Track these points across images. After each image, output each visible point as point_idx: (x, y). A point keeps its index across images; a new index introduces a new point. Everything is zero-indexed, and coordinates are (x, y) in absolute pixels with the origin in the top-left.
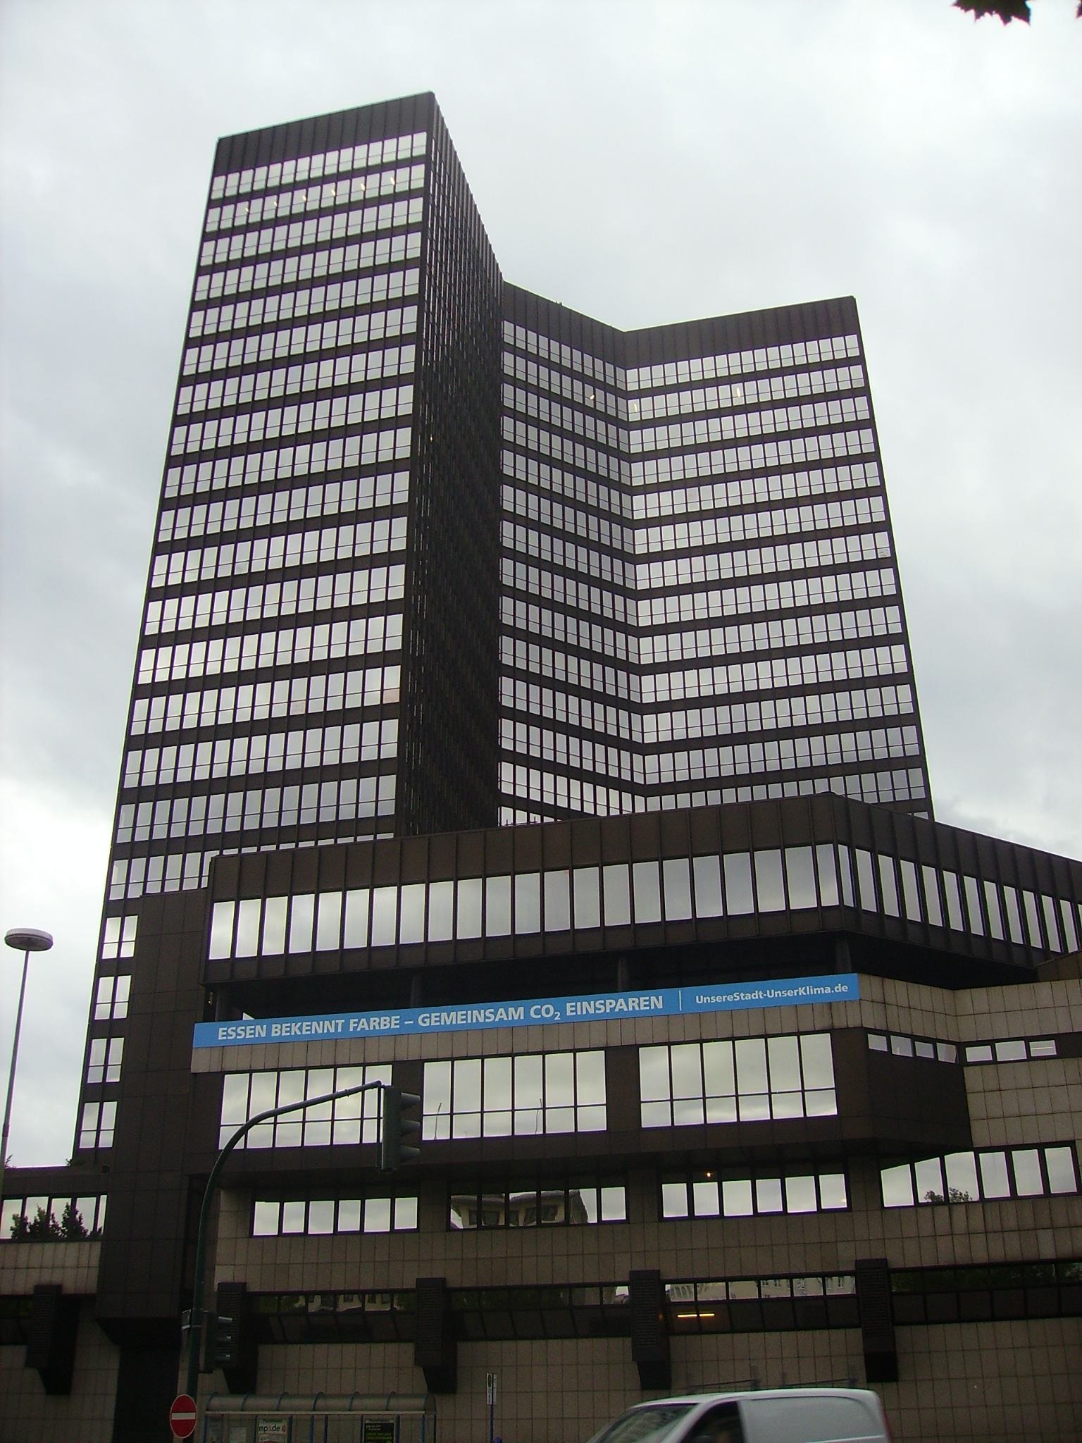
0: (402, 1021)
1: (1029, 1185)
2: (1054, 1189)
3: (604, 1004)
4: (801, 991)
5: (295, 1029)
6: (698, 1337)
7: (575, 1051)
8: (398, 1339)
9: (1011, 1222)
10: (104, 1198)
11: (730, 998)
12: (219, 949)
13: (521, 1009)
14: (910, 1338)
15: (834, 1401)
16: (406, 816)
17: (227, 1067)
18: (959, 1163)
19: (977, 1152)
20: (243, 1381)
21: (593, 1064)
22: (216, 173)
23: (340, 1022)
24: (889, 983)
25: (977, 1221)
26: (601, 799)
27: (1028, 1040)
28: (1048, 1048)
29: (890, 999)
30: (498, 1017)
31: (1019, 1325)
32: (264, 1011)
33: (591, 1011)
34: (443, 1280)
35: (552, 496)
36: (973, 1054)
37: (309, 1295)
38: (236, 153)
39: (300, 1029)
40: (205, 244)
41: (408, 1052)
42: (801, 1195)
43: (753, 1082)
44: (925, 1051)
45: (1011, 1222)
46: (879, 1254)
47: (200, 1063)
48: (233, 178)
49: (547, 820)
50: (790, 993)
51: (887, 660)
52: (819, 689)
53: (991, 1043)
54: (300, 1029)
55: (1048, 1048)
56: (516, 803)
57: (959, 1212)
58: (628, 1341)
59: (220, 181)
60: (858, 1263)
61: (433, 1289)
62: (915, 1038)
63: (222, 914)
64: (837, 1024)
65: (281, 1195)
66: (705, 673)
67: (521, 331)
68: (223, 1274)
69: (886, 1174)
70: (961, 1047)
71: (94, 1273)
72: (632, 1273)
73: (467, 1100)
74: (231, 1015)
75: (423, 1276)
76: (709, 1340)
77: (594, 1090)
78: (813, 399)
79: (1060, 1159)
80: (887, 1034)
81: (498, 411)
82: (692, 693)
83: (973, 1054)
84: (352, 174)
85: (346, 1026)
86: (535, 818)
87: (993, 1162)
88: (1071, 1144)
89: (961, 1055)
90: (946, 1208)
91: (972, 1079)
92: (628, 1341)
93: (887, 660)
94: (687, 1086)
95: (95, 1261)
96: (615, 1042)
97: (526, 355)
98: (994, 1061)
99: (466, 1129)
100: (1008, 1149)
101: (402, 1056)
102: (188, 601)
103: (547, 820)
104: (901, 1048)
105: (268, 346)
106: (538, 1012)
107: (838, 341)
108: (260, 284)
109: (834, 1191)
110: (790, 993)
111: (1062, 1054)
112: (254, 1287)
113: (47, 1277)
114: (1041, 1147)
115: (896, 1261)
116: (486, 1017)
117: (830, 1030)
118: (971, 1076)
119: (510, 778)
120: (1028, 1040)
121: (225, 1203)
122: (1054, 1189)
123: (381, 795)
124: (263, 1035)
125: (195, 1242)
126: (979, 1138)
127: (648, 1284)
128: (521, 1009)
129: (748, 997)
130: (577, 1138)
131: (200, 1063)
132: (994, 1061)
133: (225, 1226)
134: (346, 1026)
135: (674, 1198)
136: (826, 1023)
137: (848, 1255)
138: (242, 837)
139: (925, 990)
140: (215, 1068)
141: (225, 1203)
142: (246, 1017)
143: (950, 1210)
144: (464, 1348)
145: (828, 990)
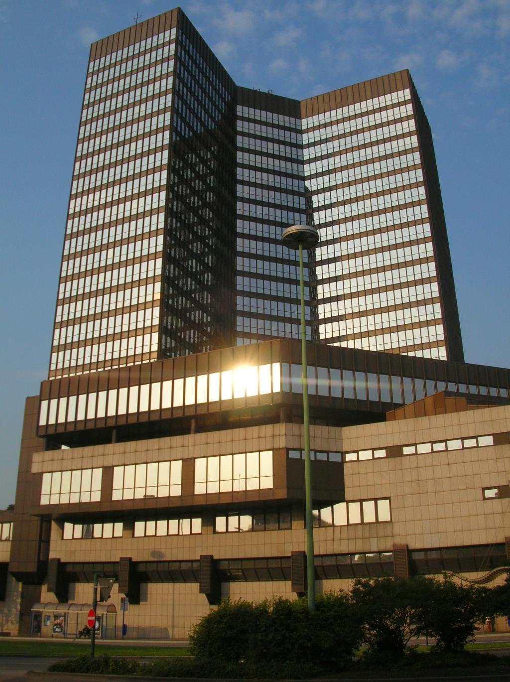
1: (369, 518)
2: (365, 521)
9: (352, 535)
10: (12, 524)
16: (162, 352)
17: (44, 471)
18: (340, 508)
19: (348, 502)
25: (345, 535)
27: (432, 443)
28: (382, 453)
35: (280, 174)
37: (353, 554)
45: (359, 535)
47: (35, 469)
55: (407, 451)
57: (337, 530)
58: (199, 584)
70: (343, 454)
71: (9, 553)
73: (213, 476)
75: (123, 556)
77: (98, 485)
78: (278, 127)
79: (384, 505)
83: (350, 457)
87: (355, 507)
88: (388, 498)
89: (343, 458)
90: (332, 528)
91: (347, 469)
92: (199, 584)
94: (213, 476)
95: (9, 549)
96: (185, 457)
100: (361, 501)
101: (106, 464)
105: (118, 118)
112: (63, 560)
114: (361, 501)
121: (54, 525)
122: (365, 521)
123: (151, 343)
125: (44, 541)
131: (35, 469)
136: (271, 447)
140: (40, 471)
141: (54, 525)
143: (333, 529)
144: (224, 585)
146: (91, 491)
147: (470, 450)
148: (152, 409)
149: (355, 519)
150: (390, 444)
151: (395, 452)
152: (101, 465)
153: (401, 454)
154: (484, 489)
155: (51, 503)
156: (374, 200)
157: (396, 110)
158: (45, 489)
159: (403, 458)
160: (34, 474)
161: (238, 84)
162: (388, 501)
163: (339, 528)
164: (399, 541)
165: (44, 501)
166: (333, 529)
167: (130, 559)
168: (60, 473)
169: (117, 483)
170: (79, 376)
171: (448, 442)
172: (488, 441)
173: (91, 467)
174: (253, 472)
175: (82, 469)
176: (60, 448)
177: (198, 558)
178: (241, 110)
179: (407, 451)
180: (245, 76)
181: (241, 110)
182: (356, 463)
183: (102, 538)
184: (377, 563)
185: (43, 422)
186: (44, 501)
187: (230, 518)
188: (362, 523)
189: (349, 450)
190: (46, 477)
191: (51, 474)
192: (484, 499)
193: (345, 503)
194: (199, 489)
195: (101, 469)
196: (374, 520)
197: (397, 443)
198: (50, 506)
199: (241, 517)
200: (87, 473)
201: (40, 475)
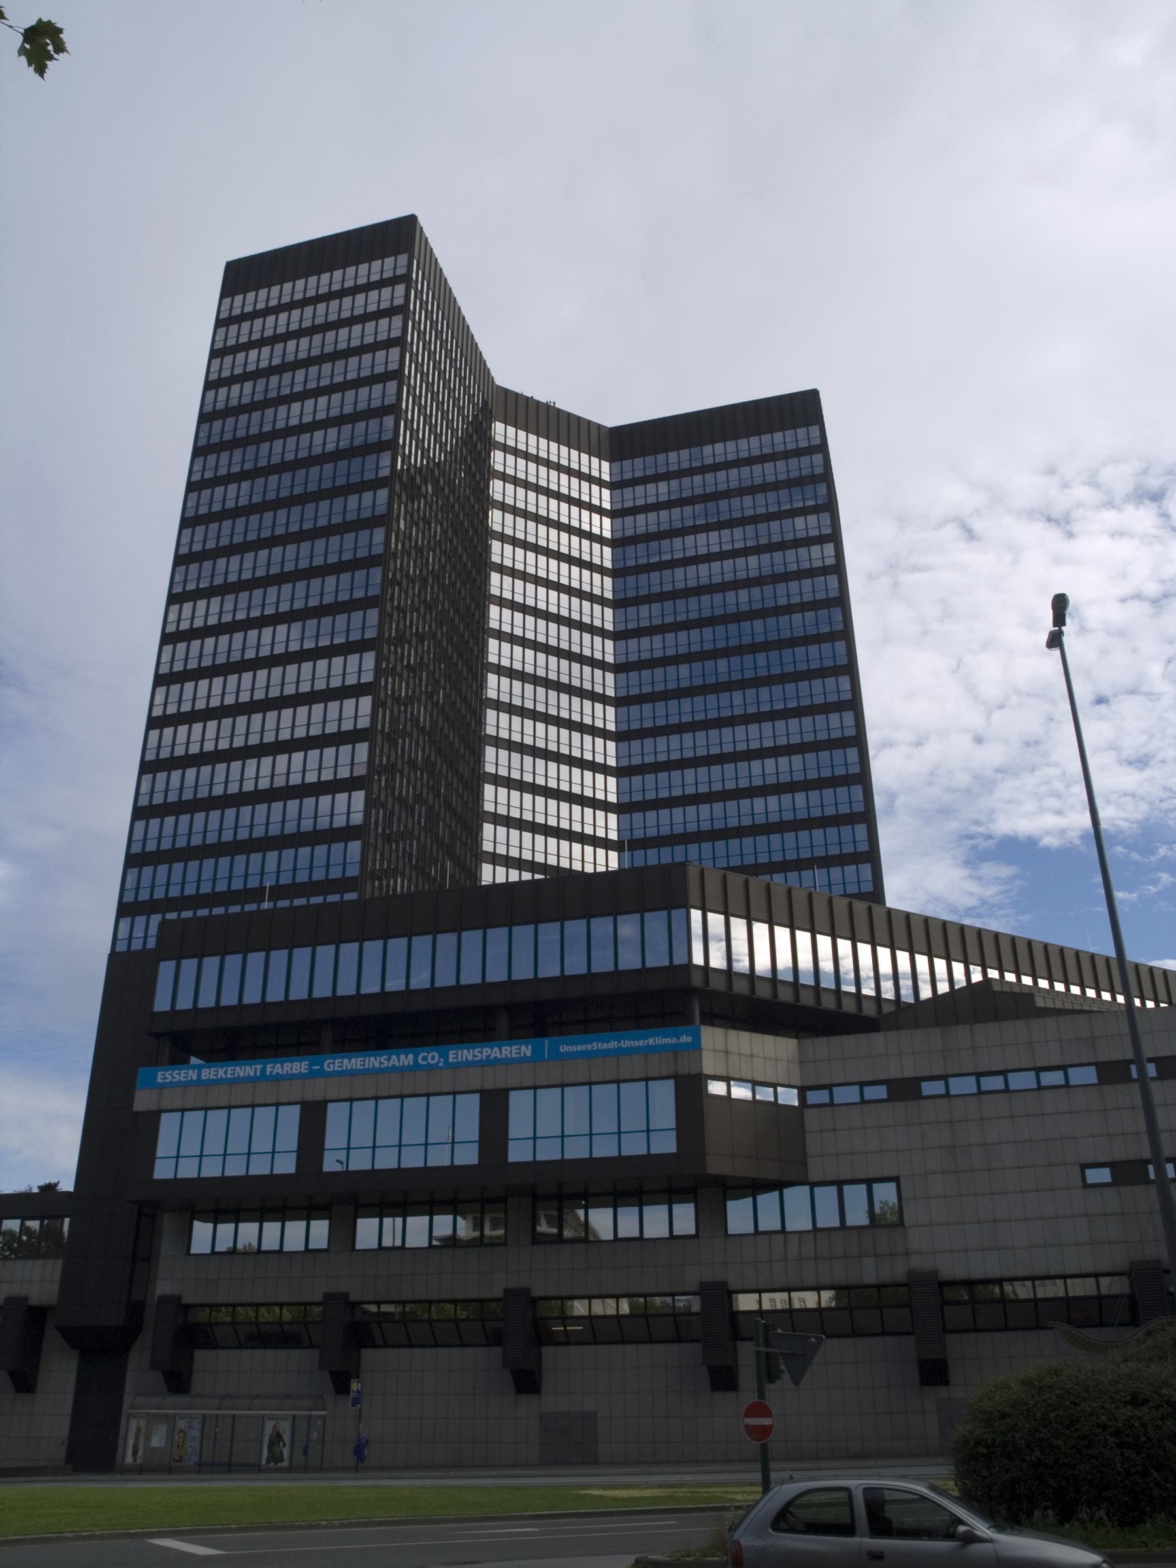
0: (310, 1066)
3: (481, 1052)
4: (651, 1041)
5: (221, 1072)
6: (566, 1347)
11: (589, 1047)
12: (161, 1003)
13: (411, 1056)
17: (164, 1106)
18: (797, 1196)
19: (813, 1185)
20: (178, 1381)
21: (470, 1106)
22: (223, 296)
23: (259, 1067)
24: (732, 1033)
26: (589, 857)
27: (979, 1075)
28: (880, 1092)
29: (730, 1048)
30: (391, 1063)
32: (212, 1056)
33: (377, 1065)
38: (242, 276)
39: (226, 1072)
40: (213, 361)
41: (315, 1091)
42: (656, 1221)
43: (606, 1123)
47: (142, 1101)
48: (238, 299)
49: (537, 876)
50: (641, 1043)
53: (829, 1087)
54: (226, 1072)
55: (928, 1088)
56: (494, 859)
59: (227, 301)
60: (702, 1284)
61: (339, 1301)
63: (166, 969)
65: (217, 1215)
66: (767, 726)
67: (511, 430)
68: (163, 1288)
69: (731, 1205)
72: (506, 1291)
73: (548, 1126)
74: (179, 1059)
76: (575, 1350)
77: (289, 1139)
80: (727, 1079)
81: (485, 502)
82: (689, 754)
84: (341, 294)
85: (263, 1070)
86: (527, 876)
87: (827, 1196)
88: (896, 1179)
94: (548, 1126)
96: (489, 1086)
97: (516, 452)
99: (548, 1152)
100: (840, 1184)
101: (309, 1097)
102: (262, 674)
103: (537, 876)
104: (741, 1092)
106: (425, 1059)
107: (801, 432)
108: (312, 385)
109: (685, 1218)
110: (641, 1043)
113: (17, 1290)
114: (840, 1184)
116: (474, 1056)
117: (676, 1077)
118: (810, 1116)
119: (492, 837)
120: (862, 1084)
124: (195, 1078)
125: (142, 1257)
126: (814, 1174)
127: (718, 1295)
128: (411, 1056)
129: (605, 1046)
130: (649, 1160)
131: (142, 1101)
132: (831, 1104)
133: (167, 1247)
134: (263, 1070)
135: (367, 1232)
137: (840, 1273)
138: (182, 902)
139: (768, 1040)
140: (153, 1107)
141: (168, 1223)
142: (194, 1060)
143: (785, 1239)
145: (674, 1040)
146: (178, 1157)
147: (932, 1101)
148: (269, 999)
149: (828, 1218)
150: (894, 1073)
151: (904, 1090)
152: (299, 1099)
153: (918, 1096)
154: (1084, 1167)
155: (179, 1176)
156: (720, 629)
157: (769, 466)
158: (165, 1145)
159: (922, 1102)
160: (137, 1113)
161: (499, 381)
162: (893, 1185)
163: (797, 1236)
164: (916, 1262)
165: (162, 1171)
166: (785, 1239)
167: (25, 1299)
168: (203, 1112)
169: (334, 1137)
170: (251, 913)
171: (835, 1089)
172: (1089, 1075)
173: (274, 1101)
174: (633, 1119)
175: (277, 1105)
176: (188, 1062)
177: (318, 1298)
178: (499, 430)
179: (928, 1088)
180: (510, 370)
181: (499, 430)
182: (829, 1109)
183: (281, 1251)
184: (1061, 1299)
185: (161, 1003)
186: (162, 1171)
187: (266, 1225)
188: (281, 1251)
189: (814, 1083)
190: (168, 1123)
191: (179, 1114)
192: (1086, 1185)
193: (806, 1188)
194: (518, 1153)
195: (671, 1083)
196: (836, 1223)
197: (909, 1073)
198: (535, 1165)
199: (312, 1222)
200: (265, 1115)
201: (152, 1120)
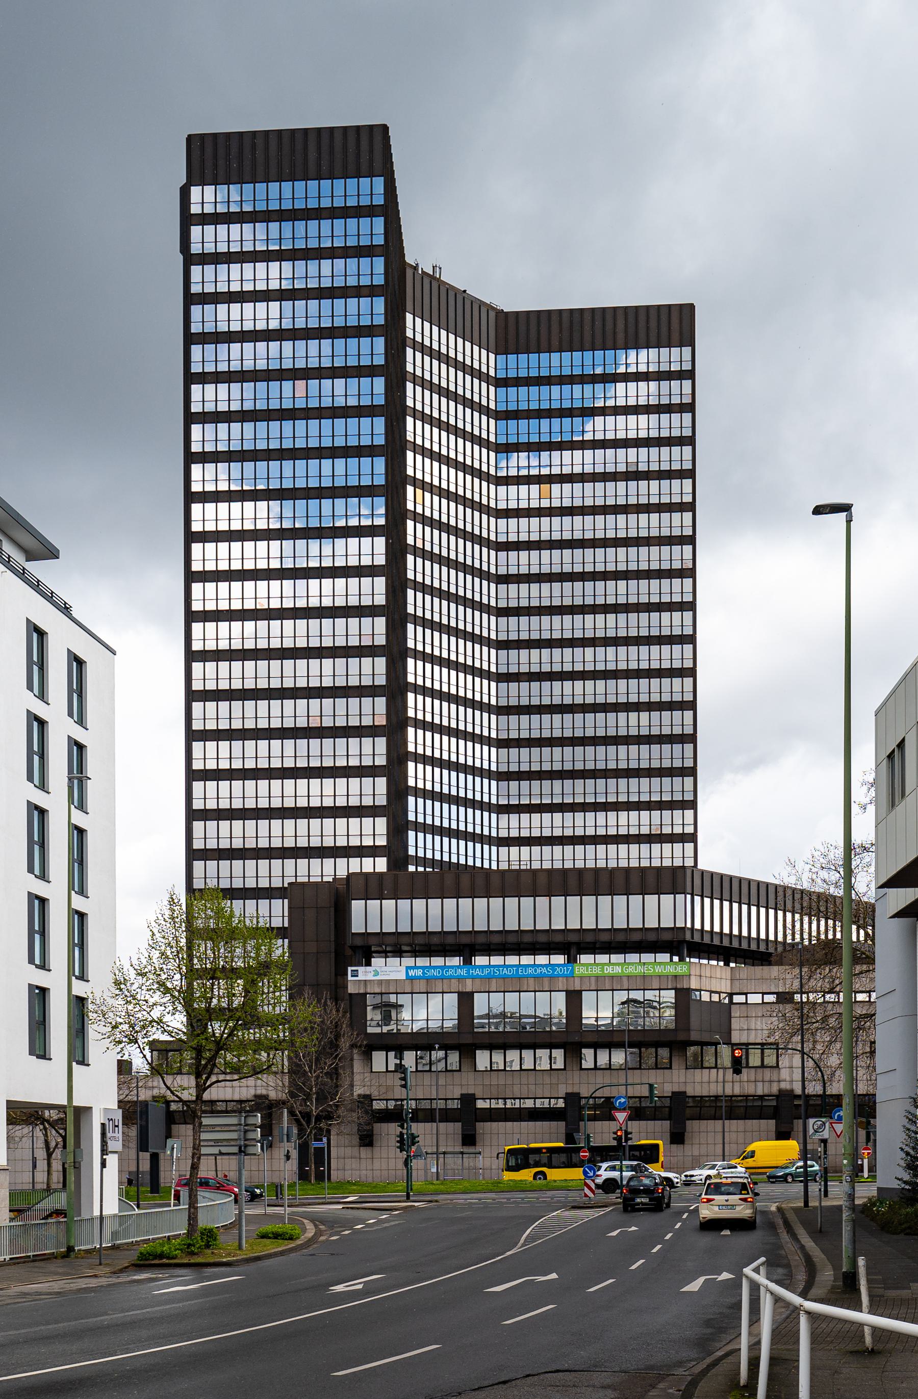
7: (551, 991)
8: (792, 1123)
14: (693, 1126)
15: (350, 1211)
31: (741, 1122)
34: (474, 1094)
36: (737, 999)
44: (715, 998)
46: (682, 1089)
51: (677, 688)
52: (552, 545)
53: (746, 994)
62: (711, 992)
64: (678, 986)
70: (731, 995)
83: (737, 999)
93: (677, 688)
98: (746, 1003)
111: (779, 1001)
115: (690, 1092)
117: (676, 989)
120: (763, 994)
132: (746, 1003)
133: (358, 1066)
